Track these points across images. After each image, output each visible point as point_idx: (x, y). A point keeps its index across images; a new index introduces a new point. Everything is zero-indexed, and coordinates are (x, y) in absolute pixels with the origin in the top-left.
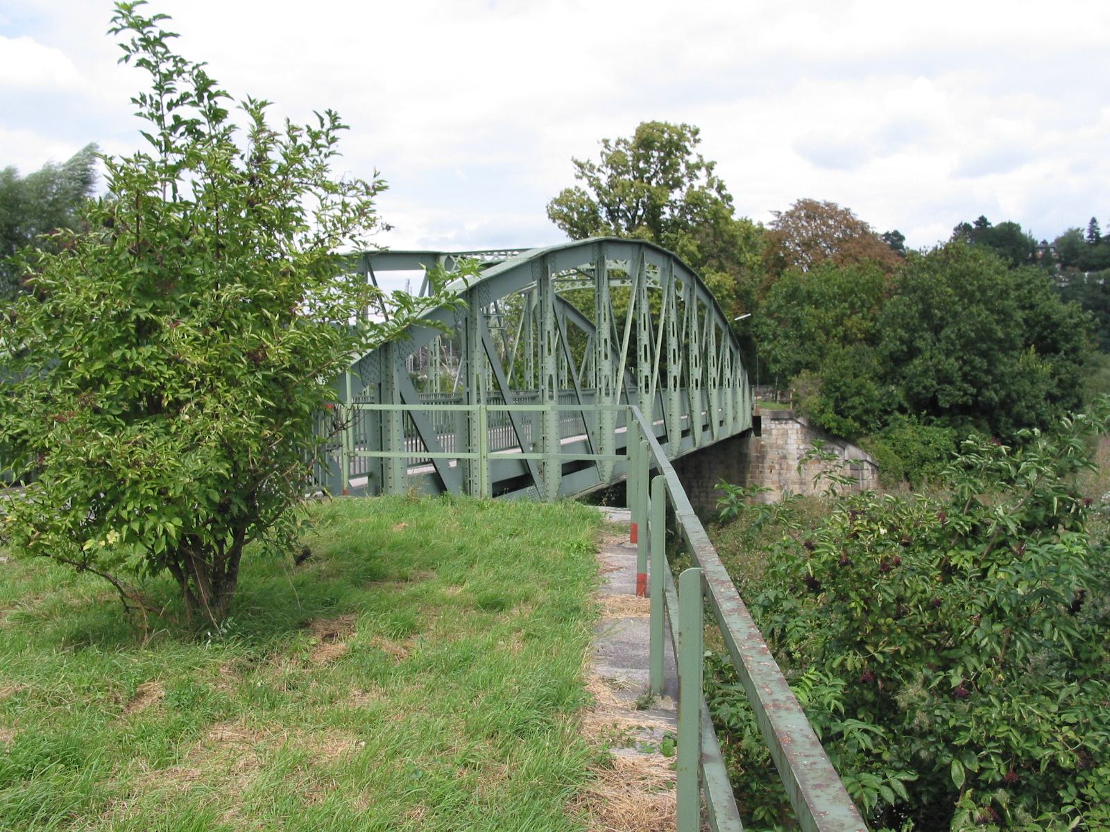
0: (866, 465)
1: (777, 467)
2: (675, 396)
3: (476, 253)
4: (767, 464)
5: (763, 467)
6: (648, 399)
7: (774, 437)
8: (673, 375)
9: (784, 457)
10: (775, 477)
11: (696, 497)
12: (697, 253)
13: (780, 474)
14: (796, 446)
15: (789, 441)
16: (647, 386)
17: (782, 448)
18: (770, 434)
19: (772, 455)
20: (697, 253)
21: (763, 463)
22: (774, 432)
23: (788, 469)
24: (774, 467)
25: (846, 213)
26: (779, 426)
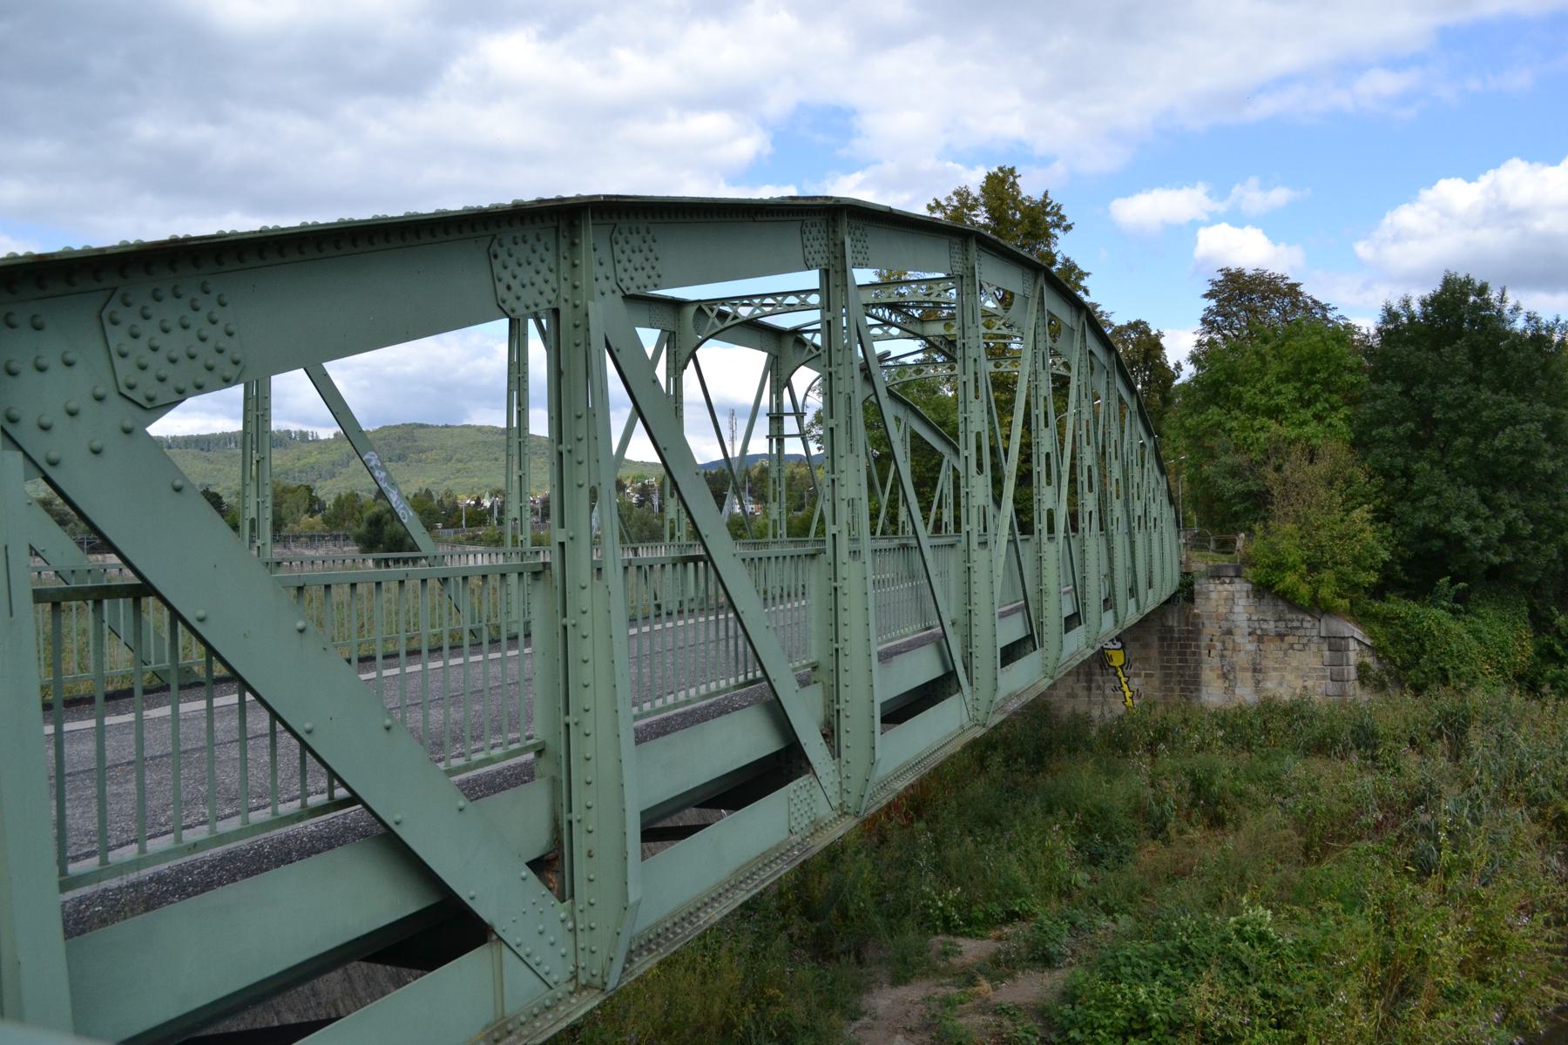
0: (1353, 645)
1: (1219, 645)
2: (1093, 543)
3: (796, 293)
4: (1204, 642)
5: (1198, 647)
6: (1053, 552)
7: (1214, 603)
8: (1087, 509)
9: (1229, 632)
10: (1216, 661)
11: (1099, 687)
12: (193, 134)
13: (1222, 656)
14: (1245, 616)
15: (1237, 609)
16: (1051, 529)
17: (1227, 620)
18: (1208, 599)
19: (1210, 629)
20: (193, 134)
21: (1197, 640)
22: (1214, 596)
23: (1234, 650)
24: (1214, 647)
25: (1293, 288)
26: (1220, 588)
